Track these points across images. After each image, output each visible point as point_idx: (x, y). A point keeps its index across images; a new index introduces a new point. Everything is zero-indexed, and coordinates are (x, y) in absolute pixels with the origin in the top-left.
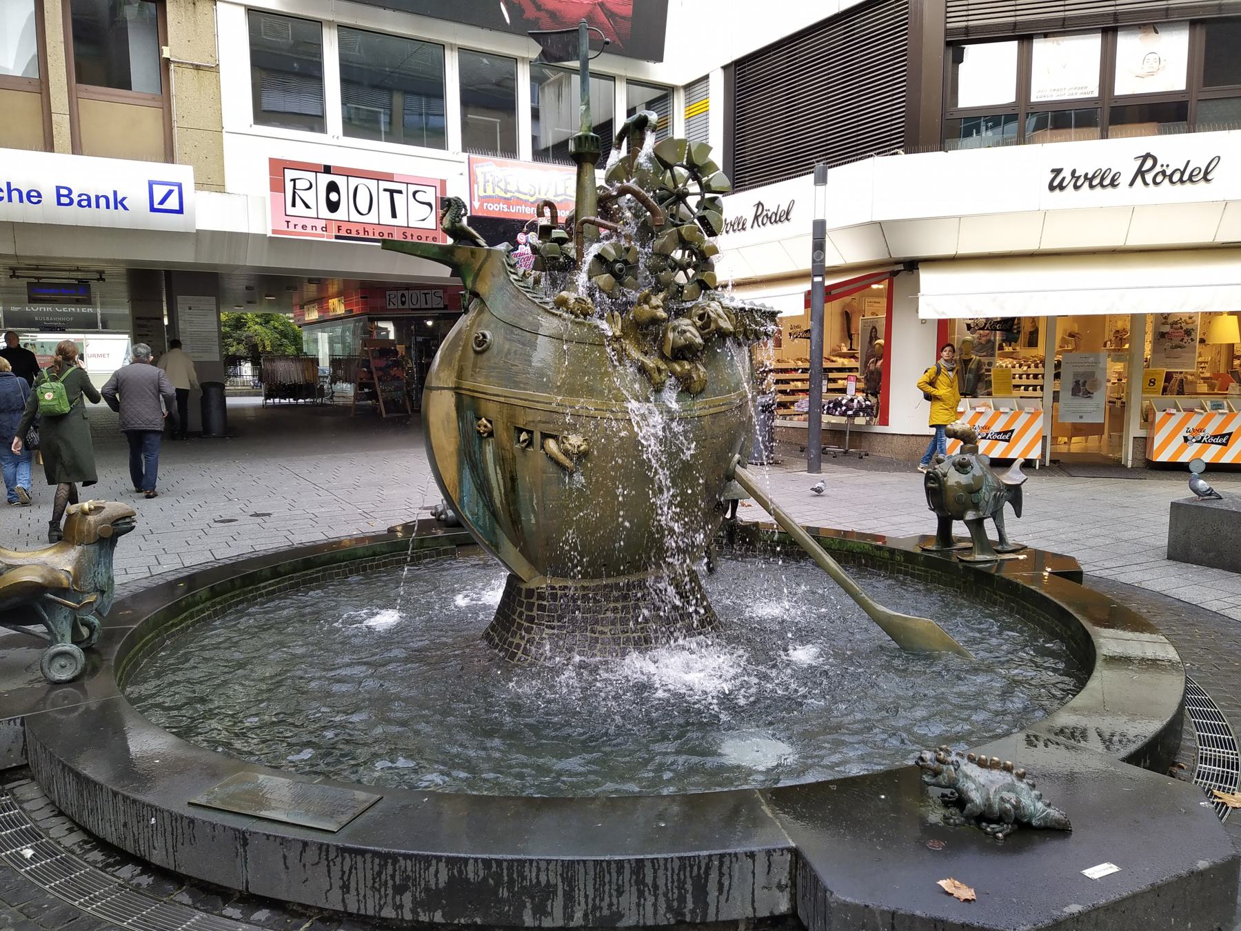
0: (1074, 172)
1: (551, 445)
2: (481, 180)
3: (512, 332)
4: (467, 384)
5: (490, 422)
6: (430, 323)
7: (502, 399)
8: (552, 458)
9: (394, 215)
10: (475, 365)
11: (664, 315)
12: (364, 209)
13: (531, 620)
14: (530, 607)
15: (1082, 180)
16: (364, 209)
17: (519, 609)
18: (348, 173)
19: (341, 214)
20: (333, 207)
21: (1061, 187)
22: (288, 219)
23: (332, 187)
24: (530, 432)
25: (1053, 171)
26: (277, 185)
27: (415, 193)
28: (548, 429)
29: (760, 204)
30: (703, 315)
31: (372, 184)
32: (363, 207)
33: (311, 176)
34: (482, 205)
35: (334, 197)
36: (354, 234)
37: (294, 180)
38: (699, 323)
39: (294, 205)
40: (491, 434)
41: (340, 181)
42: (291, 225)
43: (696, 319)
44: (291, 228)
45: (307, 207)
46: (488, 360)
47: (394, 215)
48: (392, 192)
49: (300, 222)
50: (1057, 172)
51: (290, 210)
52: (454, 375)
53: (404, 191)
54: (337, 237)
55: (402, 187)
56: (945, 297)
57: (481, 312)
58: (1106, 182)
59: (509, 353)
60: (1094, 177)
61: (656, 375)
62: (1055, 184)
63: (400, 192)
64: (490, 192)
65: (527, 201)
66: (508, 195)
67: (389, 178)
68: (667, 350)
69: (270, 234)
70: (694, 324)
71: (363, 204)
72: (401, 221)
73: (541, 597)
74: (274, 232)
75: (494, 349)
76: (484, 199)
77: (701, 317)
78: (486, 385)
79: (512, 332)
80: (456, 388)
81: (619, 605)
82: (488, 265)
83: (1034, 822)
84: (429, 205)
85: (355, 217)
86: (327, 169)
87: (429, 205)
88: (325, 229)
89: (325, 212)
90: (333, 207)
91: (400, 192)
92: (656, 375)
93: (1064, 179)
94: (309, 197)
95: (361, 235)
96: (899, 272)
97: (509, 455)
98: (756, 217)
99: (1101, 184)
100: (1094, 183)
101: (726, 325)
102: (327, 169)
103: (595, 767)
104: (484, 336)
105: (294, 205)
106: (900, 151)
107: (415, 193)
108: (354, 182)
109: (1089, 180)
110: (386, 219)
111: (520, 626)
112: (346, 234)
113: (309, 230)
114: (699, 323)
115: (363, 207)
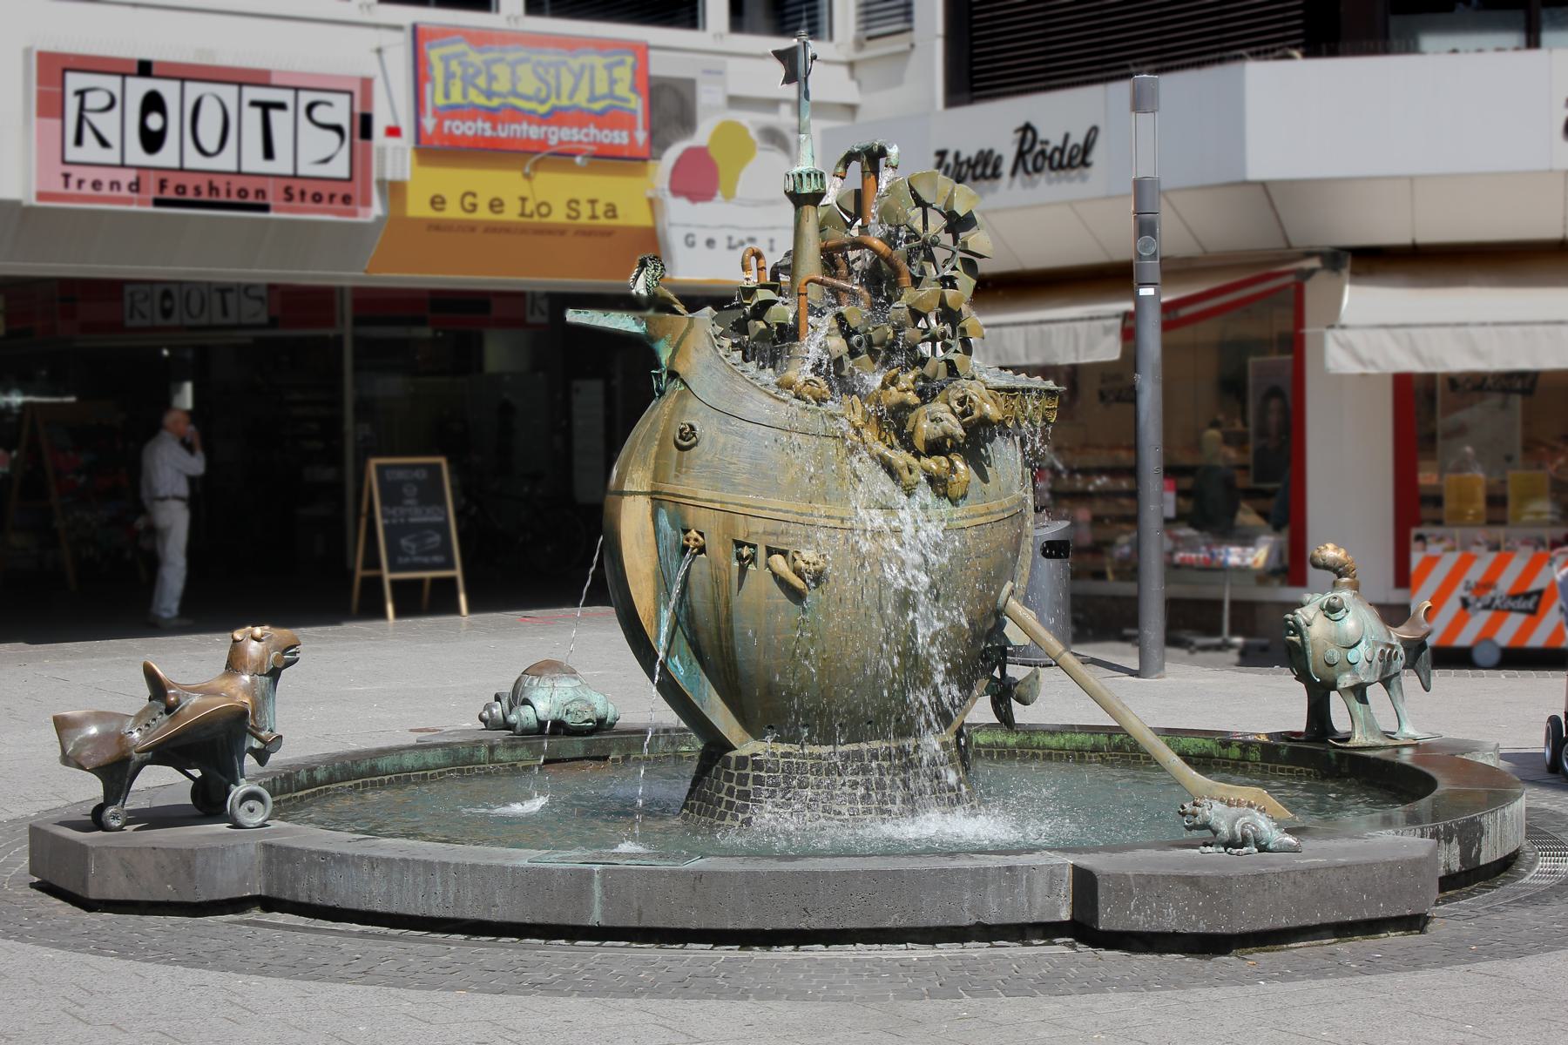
0: (957, 155)
1: (778, 560)
2: (438, 72)
3: (728, 423)
4: (667, 488)
5: (702, 534)
6: (165, 352)
7: (717, 506)
9: (269, 153)
10: (680, 464)
11: (917, 400)
12: (211, 143)
13: (745, 795)
14: (743, 780)
16: (211, 143)
17: (727, 785)
18: (183, 74)
19: (167, 156)
20: (152, 141)
22: (68, 169)
23: (153, 103)
24: (754, 547)
26: (50, 104)
27: (311, 107)
28: (772, 542)
29: (1027, 128)
31: (229, 93)
32: (210, 140)
33: (113, 83)
34: (439, 125)
35: (154, 122)
36: (190, 196)
37: (81, 93)
38: (959, 409)
39: (79, 141)
40: (702, 550)
41: (169, 90)
42: (73, 182)
43: (954, 404)
44: (73, 189)
45: (104, 143)
47: (269, 153)
48: (266, 107)
49: (90, 175)
51: (73, 153)
52: (649, 475)
53: (290, 105)
54: (158, 202)
55: (286, 96)
56: (1371, 335)
57: (681, 396)
59: (724, 449)
60: (977, 163)
61: (905, 473)
63: (281, 106)
64: (456, 97)
65: (533, 112)
66: (495, 102)
67: (261, 79)
68: (920, 446)
69: (32, 200)
70: (953, 411)
71: (209, 133)
72: (281, 164)
73: (758, 765)
74: (41, 196)
75: (704, 444)
76: (454, 111)
77: (962, 402)
78: (692, 485)
80: (653, 493)
81: (859, 778)
82: (690, 338)
83: (1271, 846)
84: (338, 129)
85: (194, 160)
86: (145, 69)
87: (338, 129)
88: (136, 186)
89: (136, 154)
90: (152, 141)
91: (281, 106)
92: (905, 473)
94: (107, 124)
95: (205, 197)
96: (1312, 272)
98: (1021, 155)
100: (979, 170)
101: (991, 410)
102: (145, 69)
103: (1050, 384)
104: (692, 428)
105: (79, 141)
106: (1296, 53)
107: (311, 107)
108: (194, 90)
110: (254, 161)
111: (730, 805)
112: (177, 194)
113: (105, 191)
114: (959, 409)
115: (210, 140)
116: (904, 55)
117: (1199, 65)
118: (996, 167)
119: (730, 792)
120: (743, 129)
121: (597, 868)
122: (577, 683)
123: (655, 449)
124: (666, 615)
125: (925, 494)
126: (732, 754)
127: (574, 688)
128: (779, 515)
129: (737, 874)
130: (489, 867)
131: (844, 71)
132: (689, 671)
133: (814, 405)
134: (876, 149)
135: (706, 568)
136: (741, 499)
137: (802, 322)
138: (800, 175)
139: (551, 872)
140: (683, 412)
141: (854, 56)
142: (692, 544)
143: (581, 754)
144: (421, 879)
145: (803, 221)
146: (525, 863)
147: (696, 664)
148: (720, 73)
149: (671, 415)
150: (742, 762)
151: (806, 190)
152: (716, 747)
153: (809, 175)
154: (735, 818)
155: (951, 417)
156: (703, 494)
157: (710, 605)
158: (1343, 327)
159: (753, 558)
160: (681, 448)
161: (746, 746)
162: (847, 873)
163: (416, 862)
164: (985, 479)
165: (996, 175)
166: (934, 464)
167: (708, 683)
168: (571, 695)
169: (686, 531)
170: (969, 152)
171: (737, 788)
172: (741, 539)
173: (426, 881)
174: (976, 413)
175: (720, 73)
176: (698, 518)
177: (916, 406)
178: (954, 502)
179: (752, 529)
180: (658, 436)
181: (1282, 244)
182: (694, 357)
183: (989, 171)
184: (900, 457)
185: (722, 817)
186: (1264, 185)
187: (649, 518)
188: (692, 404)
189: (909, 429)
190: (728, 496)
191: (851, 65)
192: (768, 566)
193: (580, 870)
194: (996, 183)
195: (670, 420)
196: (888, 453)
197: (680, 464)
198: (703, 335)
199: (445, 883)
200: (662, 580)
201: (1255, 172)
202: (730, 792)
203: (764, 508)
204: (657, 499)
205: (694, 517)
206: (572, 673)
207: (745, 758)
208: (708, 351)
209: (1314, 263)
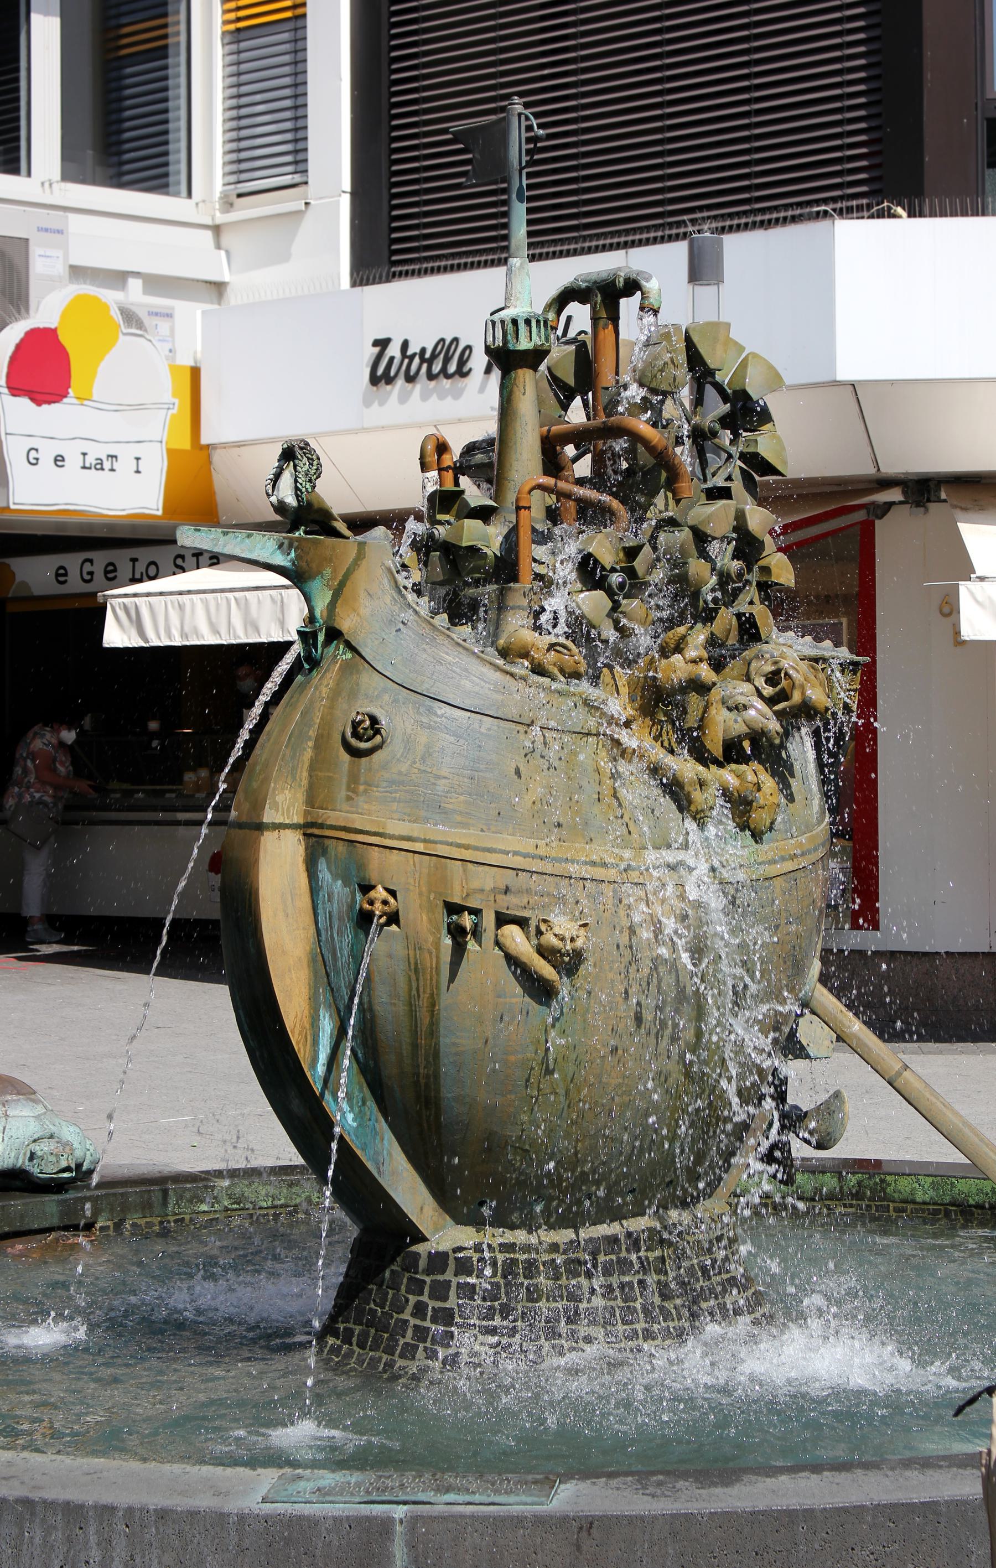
0: (405, 345)
4: (333, 817)
5: (393, 893)
7: (419, 847)
8: (512, 960)
10: (354, 779)
14: (440, 1291)
15: (417, 360)
17: (413, 1299)
21: (388, 379)
24: (476, 912)
25: (376, 343)
28: (513, 904)
30: (777, 672)
38: (768, 691)
40: (393, 918)
43: (760, 682)
46: (385, 766)
50: (382, 344)
52: (301, 796)
57: (347, 668)
58: (452, 368)
60: (434, 356)
62: (380, 371)
73: (464, 1267)
77: (773, 678)
79: (430, 710)
93: (392, 359)
96: (889, 506)
97: (428, 962)
99: (444, 371)
100: (437, 367)
104: (374, 720)
109: (426, 359)
111: (421, 1334)
114: (768, 691)
116: (297, 215)
117: (764, 225)
118: (462, 362)
119: (420, 1310)
120: (106, 307)
121: (399, 1512)
122: (40, 1109)
123: (308, 754)
124: (327, 1026)
125: (721, 823)
126: (420, 1248)
127: (37, 1117)
128: (518, 862)
129: (655, 1518)
130: (193, 1514)
131: (209, 234)
132: (360, 1116)
134: (620, 283)
135: (399, 949)
136: (458, 835)
138: (515, 322)
139: (311, 1523)
140: (353, 695)
141: (220, 218)
142: (378, 908)
143: (55, 1222)
144: (57, 1536)
145: (517, 393)
146: (252, 1502)
147: (371, 1104)
148: (60, 232)
149: (335, 695)
150: (438, 1261)
151: (524, 344)
152: (382, 1240)
153: (528, 322)
154: (432, 1355)
155: (760, 704)
156: (396, 827)
157: (402, 1009)
158: (982, 579)
159: (476, 932)
160: (355, 753)
161: (444, 1235)
162: (845, 1510)
163: (49, 1505)
164: (791, 798)
165: (462, 372)
166: (728, 776)
167: (389, 1136)
168: (33, 1129)
169: (366, 888)
170: (423, 340)
171: (432, 1304)
172: (457, 900)
173: (69, 1540)
174: (796, 697)
175: (60, 232)
176: (386, 867)
178: (757, 836)
179: (475, 884)
180: (312, 733)
182: (366, 606)
183: (452, 368)
184: (684, 766)
185: (409, 1351)
187: (302, 867)
188: (368, 681)
190: (439, 830)
191: (217, 229)
192: (497, 943)
193: (368, 1519)
194: (460, 382)
195: (332, 707)
197: (354, 779)
198: (380, 572)
199: (106, 1543)
200: (324, 965)
201: (844, 374)
202: (420, 1310)
203: (495, 850)
204: (316, 839)
205: (378, 864)
206: (24, 1091)
207: (444, 1255)
208: (387, 596)
209: (895, 495)
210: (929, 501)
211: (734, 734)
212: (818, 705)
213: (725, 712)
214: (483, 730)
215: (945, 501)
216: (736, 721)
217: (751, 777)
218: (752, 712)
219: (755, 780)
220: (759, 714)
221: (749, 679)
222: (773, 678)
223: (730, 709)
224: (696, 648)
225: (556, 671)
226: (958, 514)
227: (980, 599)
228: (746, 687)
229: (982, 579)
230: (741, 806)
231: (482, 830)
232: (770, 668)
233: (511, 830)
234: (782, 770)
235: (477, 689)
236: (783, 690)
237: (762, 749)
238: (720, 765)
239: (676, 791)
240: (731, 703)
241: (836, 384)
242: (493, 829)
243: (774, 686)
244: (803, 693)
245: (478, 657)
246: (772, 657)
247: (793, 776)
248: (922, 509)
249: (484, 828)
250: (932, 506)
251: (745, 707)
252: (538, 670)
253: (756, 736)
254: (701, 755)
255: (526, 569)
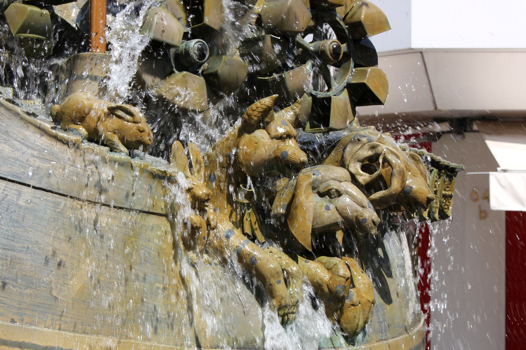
11: (303, 157)
38: (364, 177)
43: (356, 167)
70: (354, 180)
96: (439, 135)
114: (364, 177)
133: (123, 154)
137: (97, 22)
158: (505, 171)
164: (385, 295)
166: (317, 268)
174: (395, 185)
177: (303, 165)
181: (432, 108)
184: (271, 257)
186: (421, 52)
189: (279, 208)
196: (248, 247)
201: (416, 44)
210: (465, 131)
211: (327, 222)
212: (419, 195)
213: (316, 198)
214: (21, 202)
215: (477, 131)
216: (328, 208)
217: (343, 271)
218: (346, 200)
219: (348, 274)
220: (355, 202)
221: (343, 164)
222: (369, 164)
223: (321, 195)
224: (283, 124)
225: (116, 139)
226: (485, 136)
227: (503, 184)
228: (341, 172)
229: (505, 171)
230: (331, 300)
231: (13, 321)
232: (366, 153)
233: (49, 322)
234: (380, 269)
235: (17, 154)
236: (380, 176)
237: (358, 241)
238: (309, 256)
239: (261, 287)
240: (322, 189)
241: (411, 51)
242: (26, 319)
243: (371, 172)
244: (403, 181)
245: (22, 119)
246: (370, 141)
247: (390, 275)
248: (461, 136)
249: (16, 318)
250: (467, 135)
251: (339, 194)
252: (94, 137)
253: (353, 226)
254: (293, 250)
255: (98, 41)
